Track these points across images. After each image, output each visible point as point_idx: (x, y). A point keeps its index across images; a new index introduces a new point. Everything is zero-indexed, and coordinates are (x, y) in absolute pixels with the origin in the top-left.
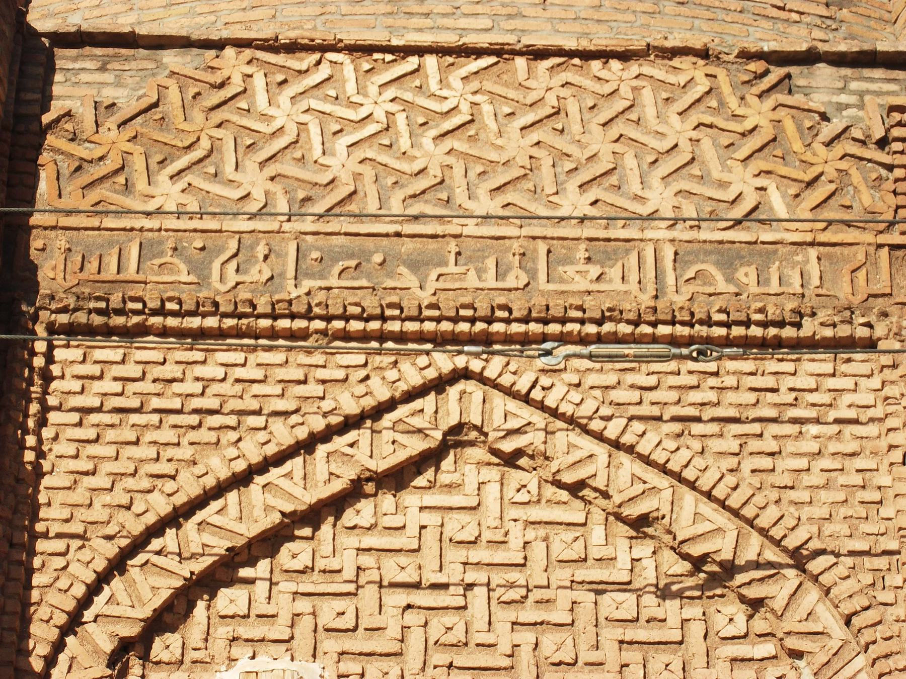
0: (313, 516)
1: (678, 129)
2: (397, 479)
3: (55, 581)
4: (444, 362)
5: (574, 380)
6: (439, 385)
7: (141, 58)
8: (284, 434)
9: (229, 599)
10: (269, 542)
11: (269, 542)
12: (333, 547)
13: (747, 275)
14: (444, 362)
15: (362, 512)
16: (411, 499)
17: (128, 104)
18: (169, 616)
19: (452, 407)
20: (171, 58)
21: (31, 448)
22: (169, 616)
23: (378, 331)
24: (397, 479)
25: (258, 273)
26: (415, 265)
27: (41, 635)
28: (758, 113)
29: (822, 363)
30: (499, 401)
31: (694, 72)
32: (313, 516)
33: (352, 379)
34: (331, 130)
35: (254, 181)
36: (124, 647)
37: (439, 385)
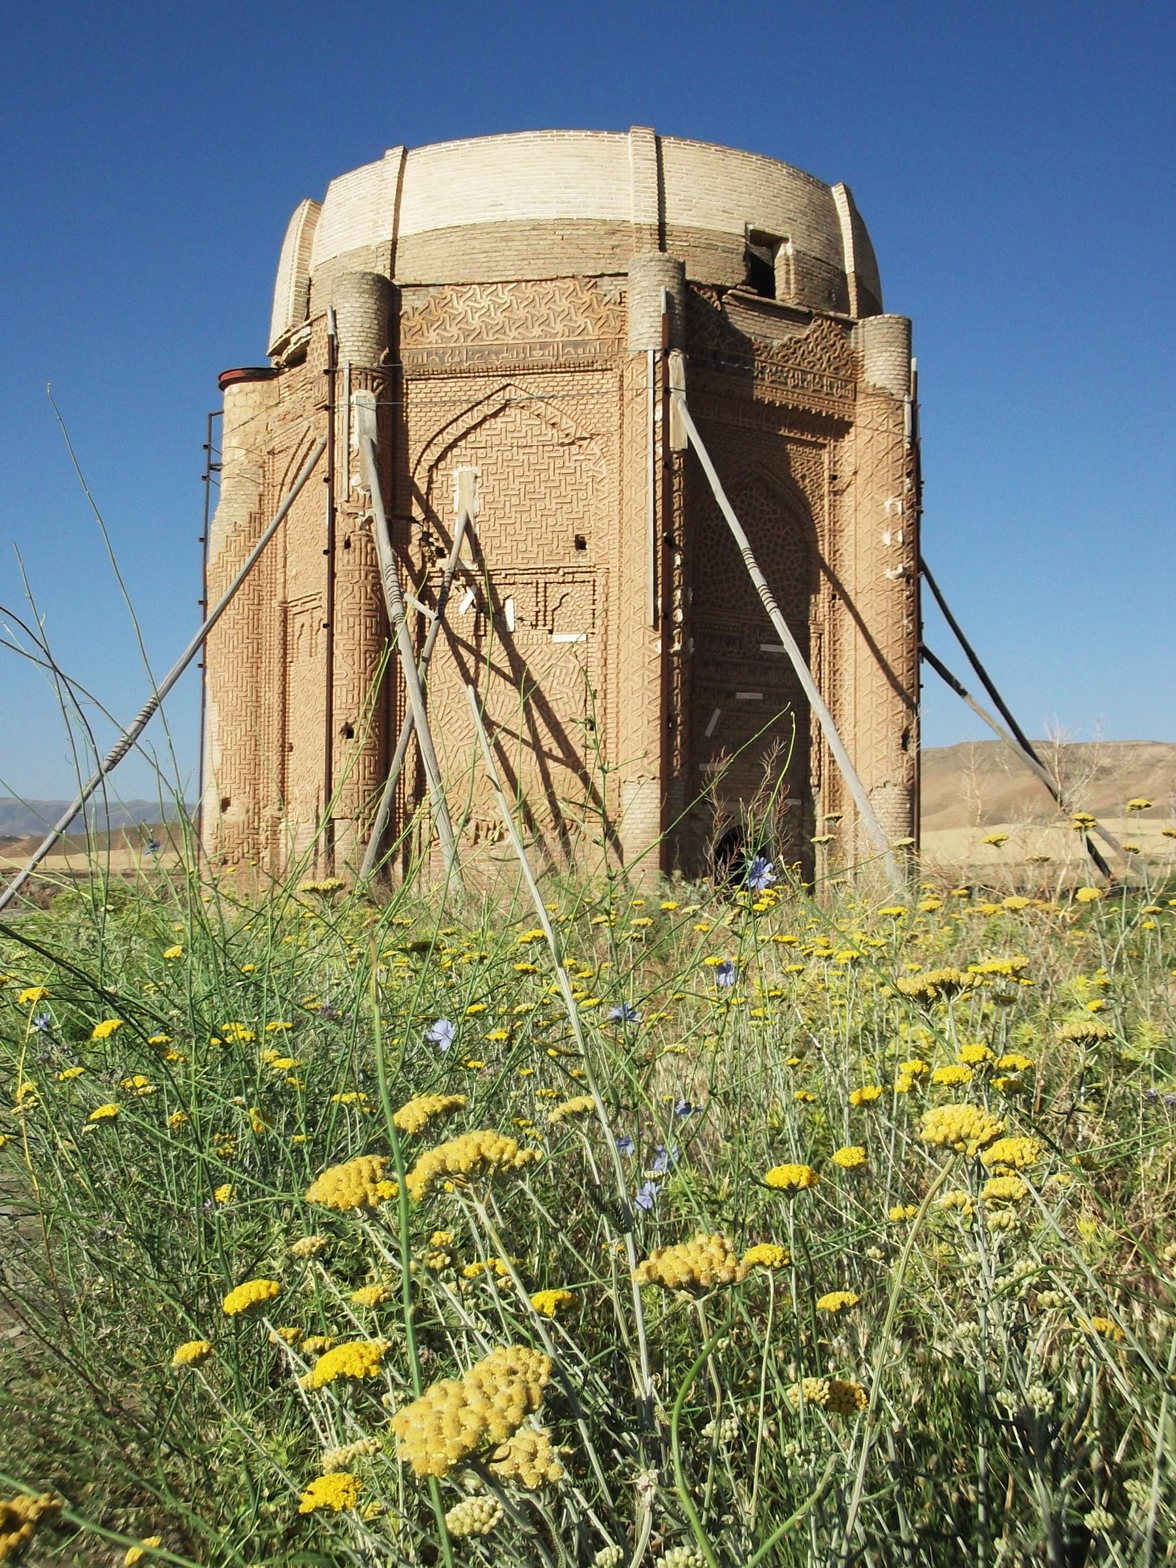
0: (475, 427)
1: (565, 304)
2: (495, 415)
3: (414, 452)
4: (505, 381)
5: (534, 385)
6: (504, 388)
7: (423, 291)
8: (466, 407)
9: (456, 451)
10: (464, 436)
11: (464, 436)
12: (479, 436)
13: (580, 351)
14: (505, 381)
15: (486, 425)
16: (498, 420)
17: (421, 308)
18: (442, 457)
19: (507, 394)
20: (431, 289)
21: (880, 393)
22: (442, 457)
23: (487, 373)
24: (495, 415)
25: (457, 359)
26: (497, 354)
27: (412, 466)
28: (586, 297)
29: (598, 375)
30: (519, 392)
31: (569, 283)
32: (475, 427)
33: (480, 387)
34: (475, 308)
35: (454, 331)
36: (431, 467)
37: (504, 388)
